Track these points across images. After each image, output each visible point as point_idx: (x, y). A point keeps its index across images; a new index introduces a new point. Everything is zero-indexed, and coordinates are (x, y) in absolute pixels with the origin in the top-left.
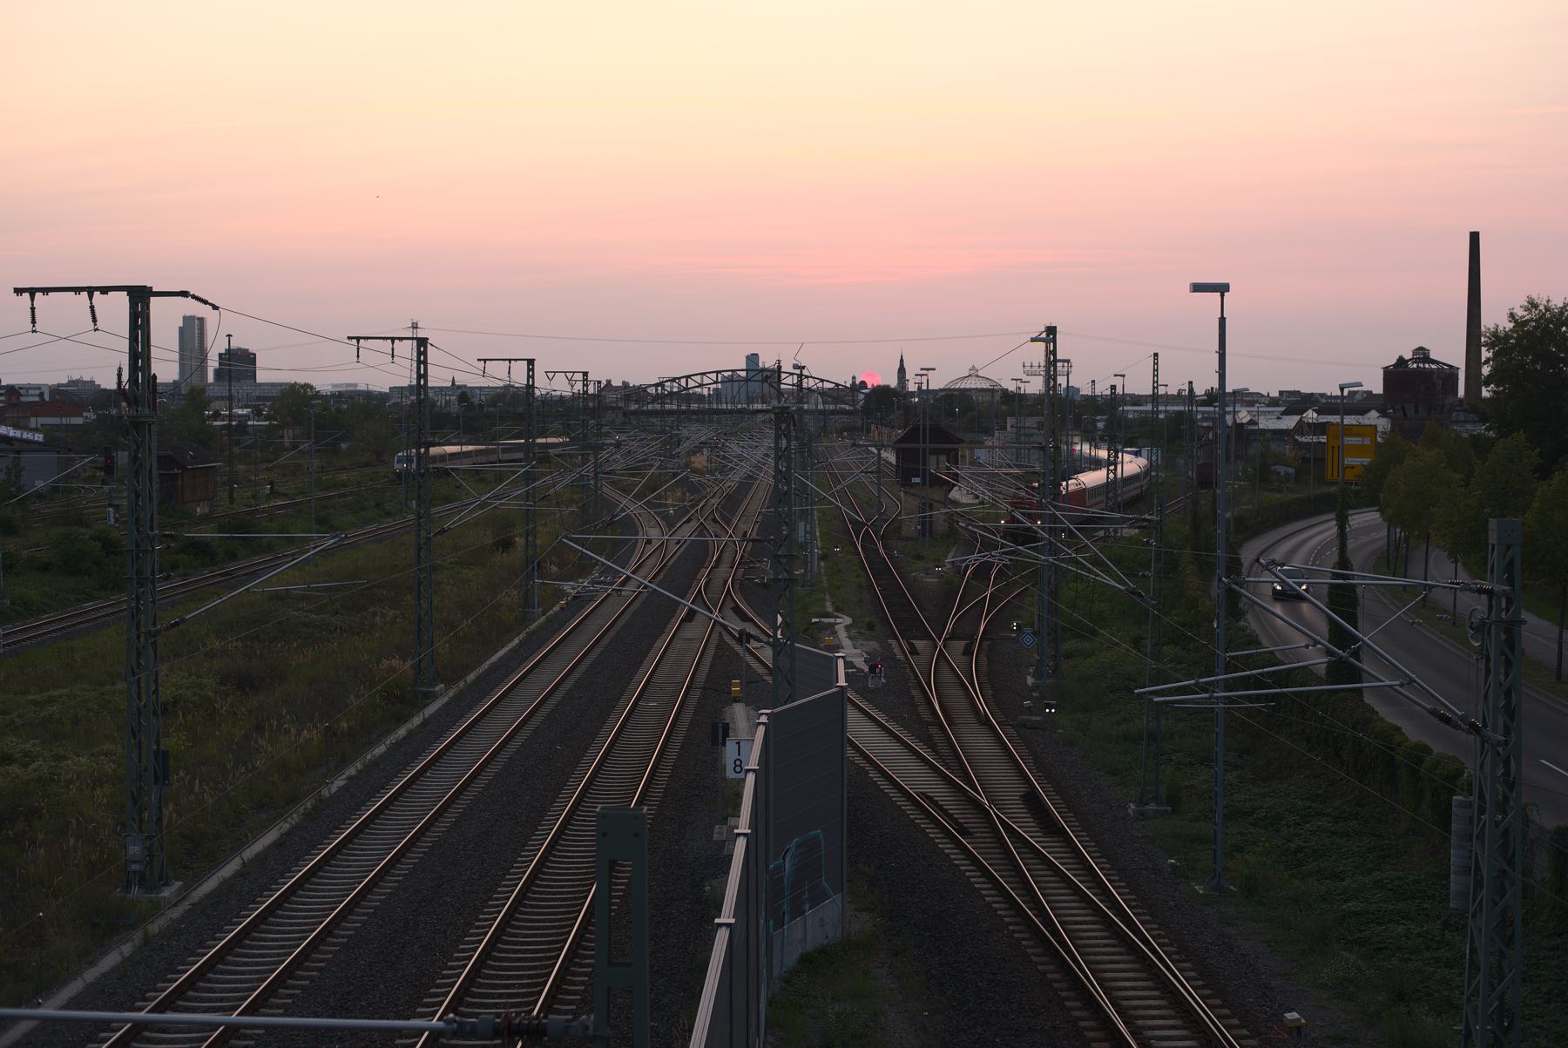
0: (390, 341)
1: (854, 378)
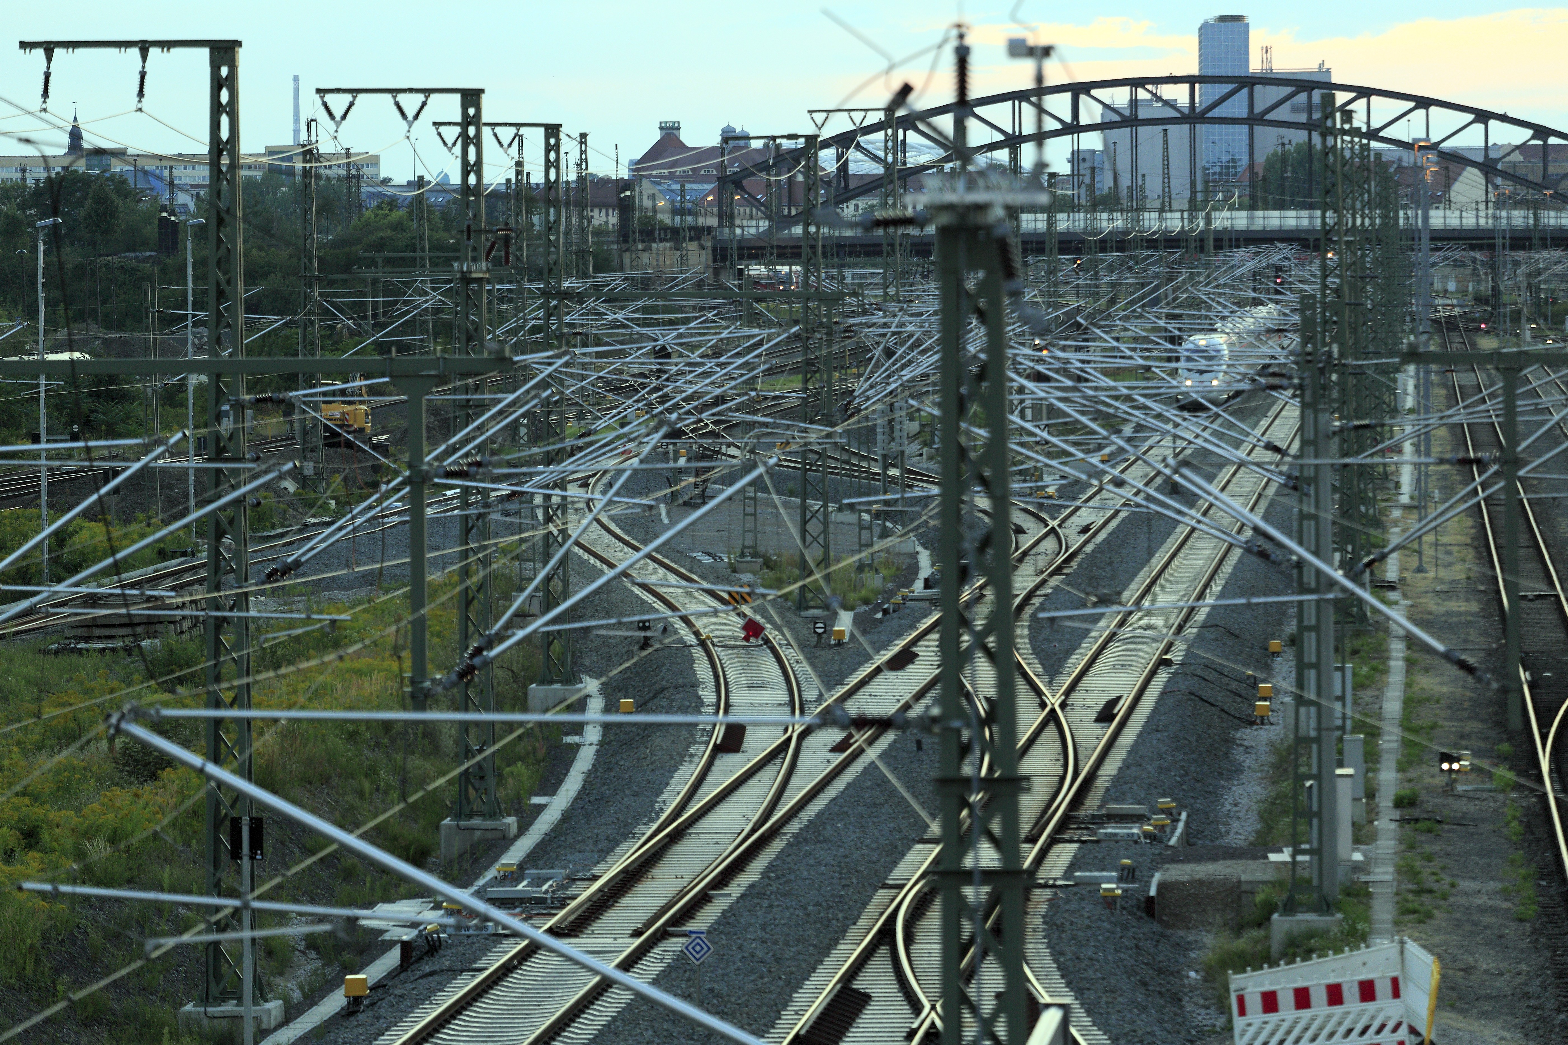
0: (135, 52)
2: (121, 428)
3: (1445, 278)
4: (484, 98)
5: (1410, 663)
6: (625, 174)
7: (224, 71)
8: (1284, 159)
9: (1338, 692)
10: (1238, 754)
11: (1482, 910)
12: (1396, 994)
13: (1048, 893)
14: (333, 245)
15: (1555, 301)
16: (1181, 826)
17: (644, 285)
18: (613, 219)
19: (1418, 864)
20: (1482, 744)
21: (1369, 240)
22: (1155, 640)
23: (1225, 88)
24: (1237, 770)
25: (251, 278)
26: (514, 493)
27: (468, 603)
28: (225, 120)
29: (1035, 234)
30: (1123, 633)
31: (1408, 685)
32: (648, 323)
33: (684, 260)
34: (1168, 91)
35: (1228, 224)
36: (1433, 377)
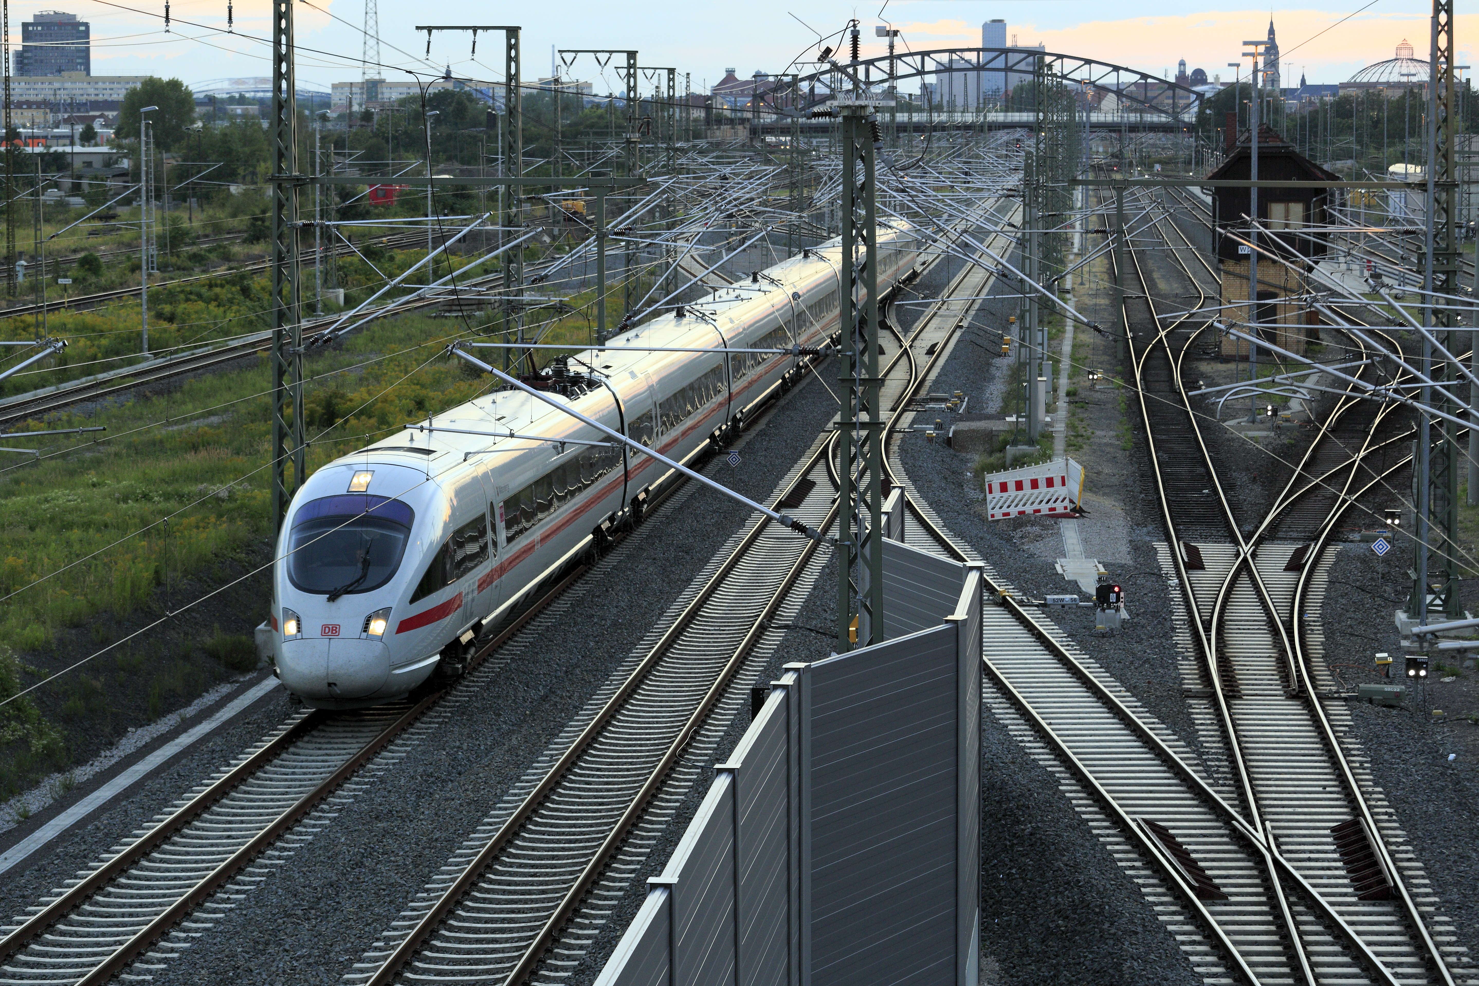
0: (471, 31)
1: (1182, 64)
2: (468, 211)
3: (1098, 145)
4: (638, 55)
5: (1076, 328)
6: (709, 93)
7: (513, 41)
8: (1021, 88)
9: (1040, 340)
10: (993, 370)
11: (1106, 445)
12: (1064, 484)
13: (901, 435)
14: (570, 125)
15: (1149, 157)
16: (965, 404)
17: (717, 146)
18: (703, 114)
19: (1076, 423)
20: (1108, 367)
21: (1060, 127)
22: (955, 316)
23: (994, 54)
24: (993, 378)
25: (527, 141)
26: (650, 244)
27: (629, 296)
28: (513, 64)
29: (903, 123)
30: (940, 313)
31: (1074, 338)
32: (719, 163)
33: (736, 134)
34: (967, 55)
35: (994, 119)
36: (1090, 193)
